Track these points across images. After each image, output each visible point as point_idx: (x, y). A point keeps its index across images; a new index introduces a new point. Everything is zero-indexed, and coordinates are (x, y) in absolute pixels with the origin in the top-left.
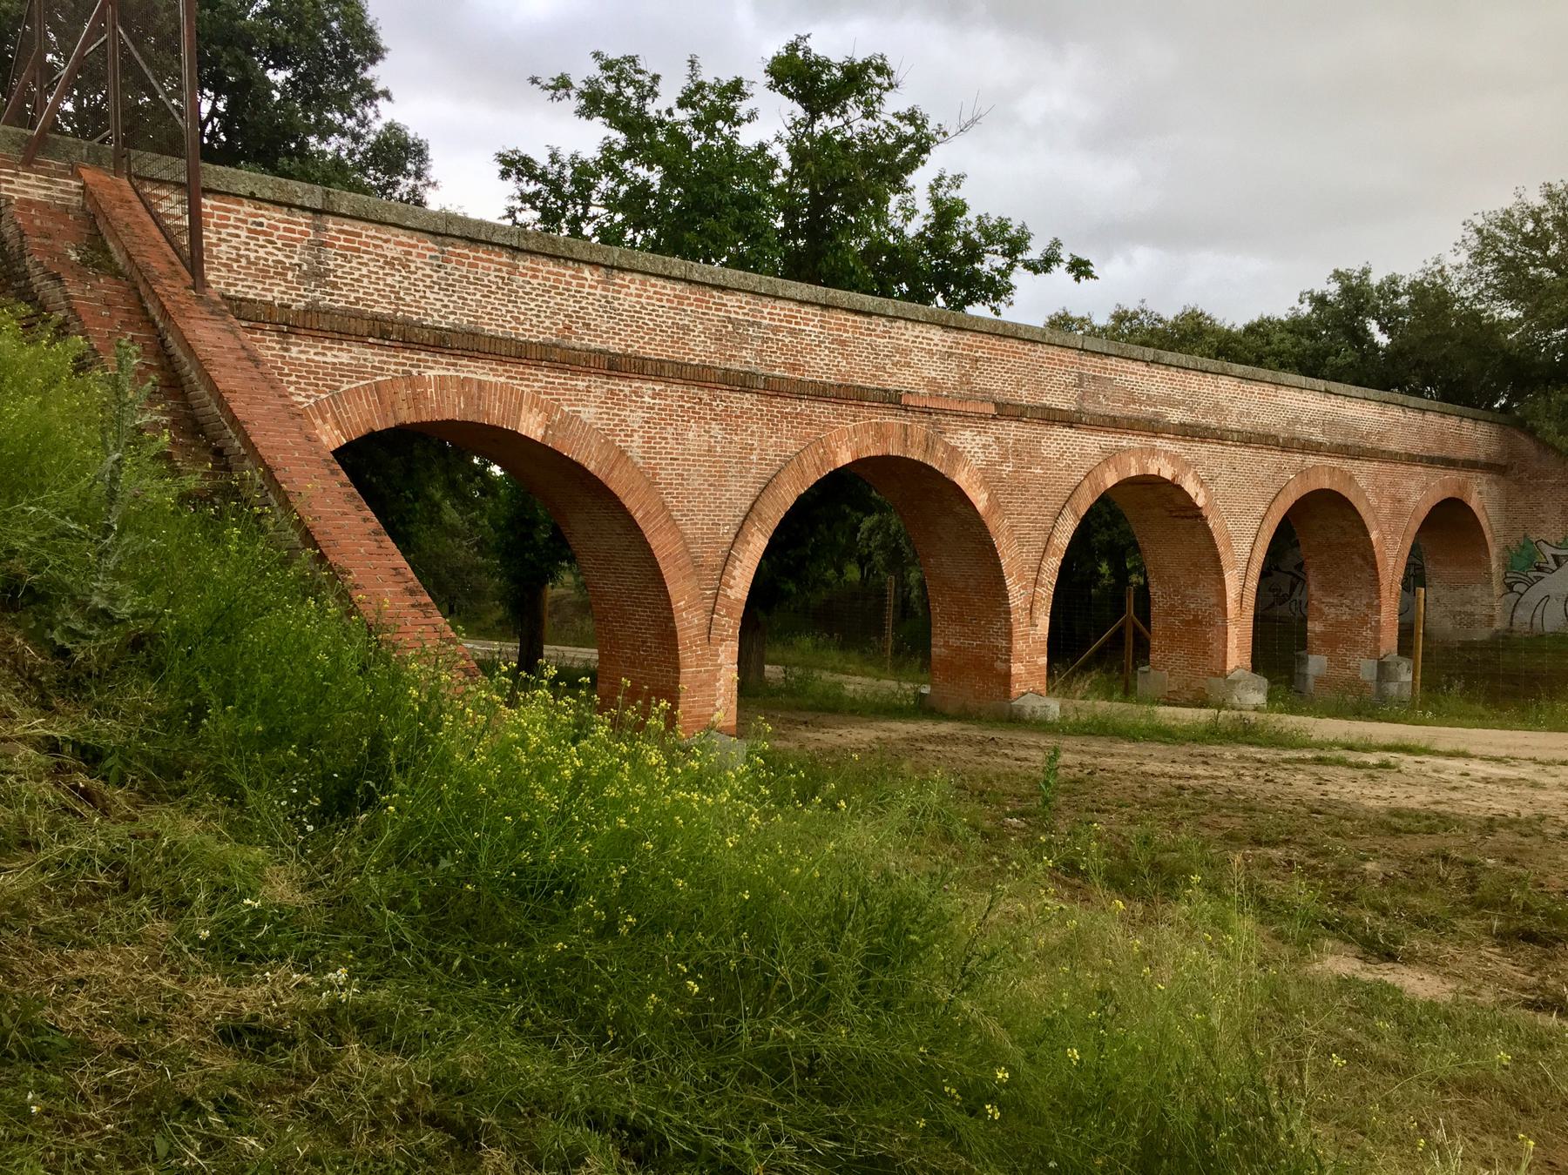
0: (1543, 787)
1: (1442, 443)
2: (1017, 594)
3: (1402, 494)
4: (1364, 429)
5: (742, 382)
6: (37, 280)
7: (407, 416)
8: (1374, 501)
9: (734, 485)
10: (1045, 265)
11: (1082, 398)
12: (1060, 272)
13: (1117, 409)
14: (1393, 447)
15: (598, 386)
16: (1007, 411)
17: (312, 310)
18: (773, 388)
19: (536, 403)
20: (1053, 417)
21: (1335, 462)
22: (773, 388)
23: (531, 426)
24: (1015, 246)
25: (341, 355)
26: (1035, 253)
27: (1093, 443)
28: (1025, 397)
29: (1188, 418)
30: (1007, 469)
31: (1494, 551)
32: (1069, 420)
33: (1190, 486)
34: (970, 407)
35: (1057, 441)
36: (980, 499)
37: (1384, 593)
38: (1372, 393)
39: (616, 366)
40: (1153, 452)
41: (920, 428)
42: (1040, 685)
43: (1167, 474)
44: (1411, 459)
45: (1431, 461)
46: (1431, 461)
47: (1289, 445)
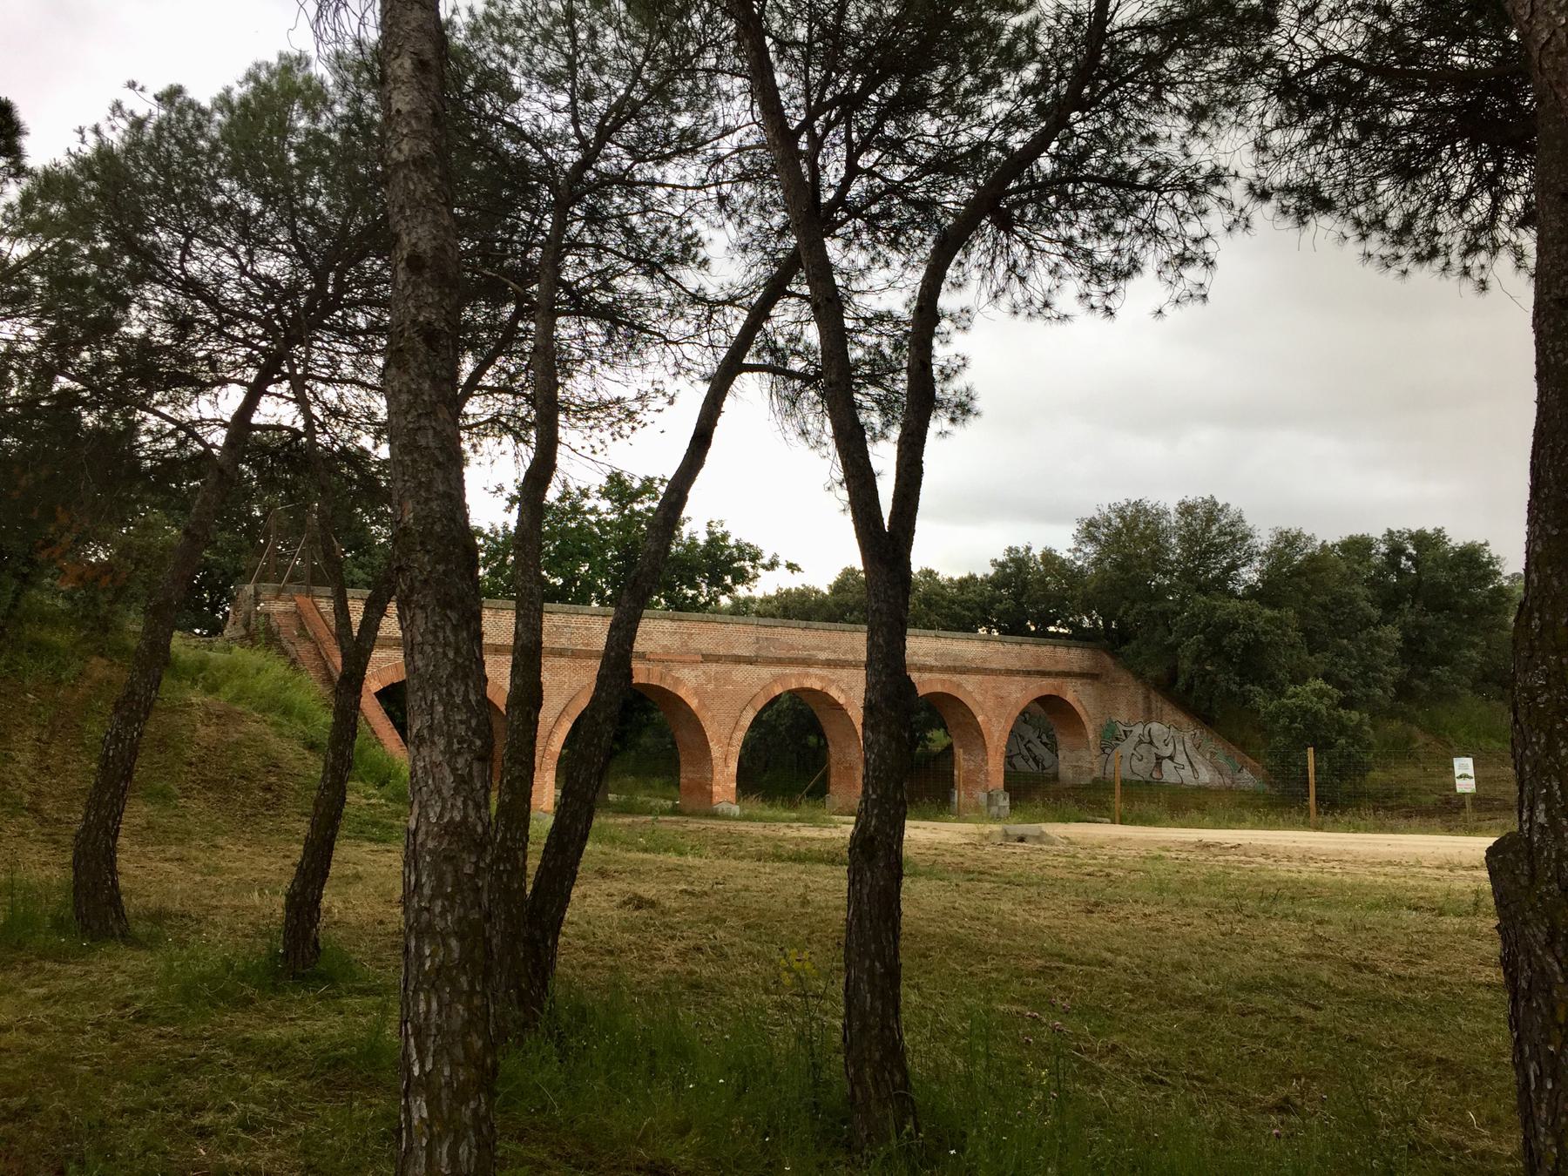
0: (1329, 922)
1: (1039, 662)
2: (716, 751)
3: (1003, 693)
4: (970, 656)
6: (285, 643)
8: (979, 698)
10: (773, 565)
11: (759, 649)
12: (781, 570)
13: (782, 654)
14: (994, 666)
16: (708, 658)
20: (738, 660)
21: (946, 677)
24: (755, 557)
26: (765, 561)
27: (766, 672)
28: (722, 651)
29: (832, 656)
30: (711, 687)
31: (1090, 728)
32: (750, 661)
33: (834, 692)
34: (686, 658)
35: (741, 673)
36: (693, 703)
37: (991, 752)
38: (958, 634)
40: (807, 675)
41: (657, 669)
42: (732, 798)
43: (817, 686)
44: (1010, 672)
45: (1028, 673)
46: (1028, 673)
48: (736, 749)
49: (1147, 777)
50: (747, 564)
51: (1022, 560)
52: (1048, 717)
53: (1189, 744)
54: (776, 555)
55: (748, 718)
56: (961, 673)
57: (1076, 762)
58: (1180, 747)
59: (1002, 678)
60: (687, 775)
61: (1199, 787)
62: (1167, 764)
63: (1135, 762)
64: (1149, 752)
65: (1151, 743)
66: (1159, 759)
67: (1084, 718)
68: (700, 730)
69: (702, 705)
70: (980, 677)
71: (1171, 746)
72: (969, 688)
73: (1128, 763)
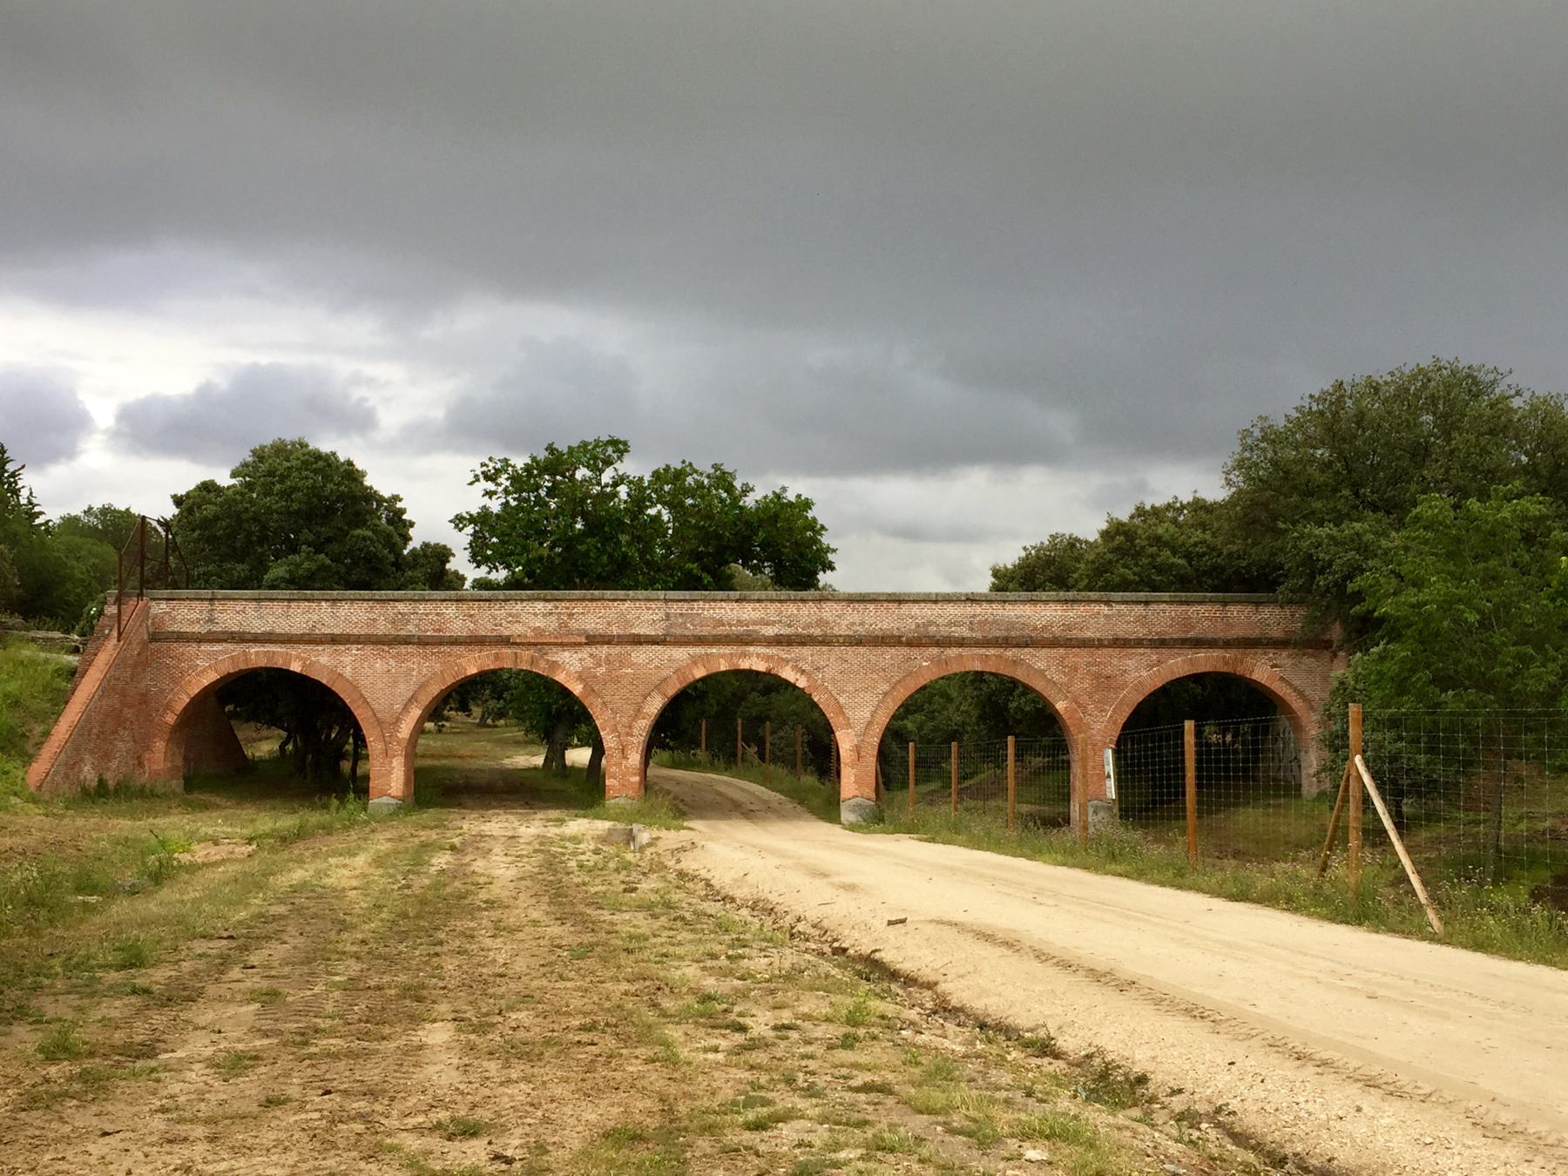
5: (406, 641)
7: (243, 667)
9: (402, 686)
15: (329, 649)
16: (593, 640)
17: (209, 632)
18: (423, 642)
19: (298, 657)
20: (638, 641)
21: (983, 651)
22: (423, 642)
23: (296, 667)
25: (218, 647)
27: (681, 654)
39: (334, 640)
47: (916, 642)
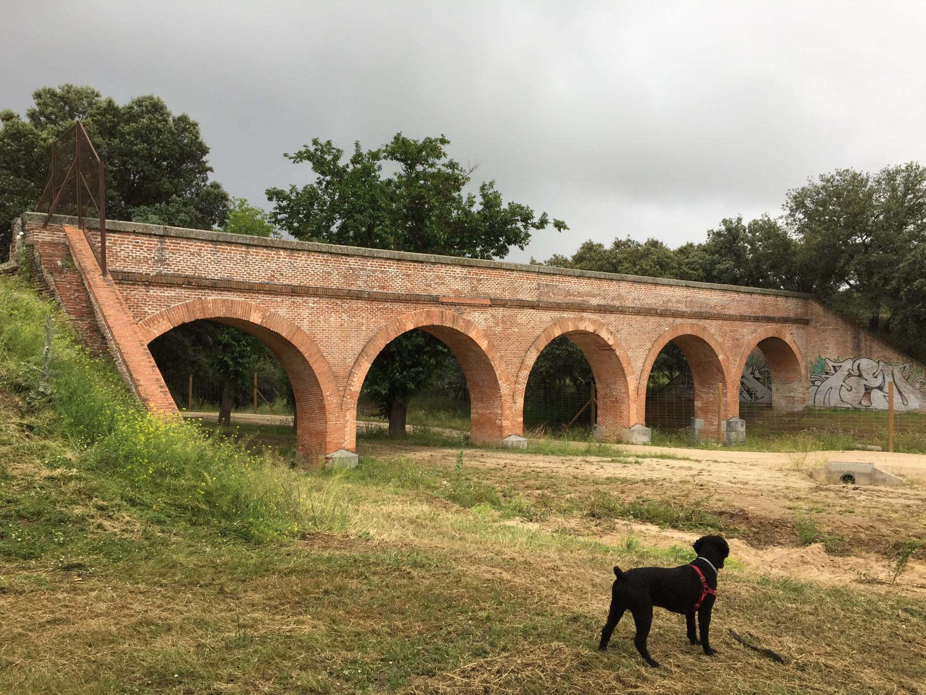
2: (504, 388)
4: (713, 304)
8: (720, 340)
10: (542, 224)
13: (560, 299)
14: (731, 312)
16: (496, 303)
20: (522, 305)
21: (694, 321)
26: (536, 220)
28: (507, 296)
30: (498, 329)
32: (533, 306)
33: (604, 335)
35: (524, 316)
36: (484, 344)
37: (729, 386)
40: (582, 319)
41: (450, 312)
43: (590, 329)
44: (743, 318)
45: (757, 319)
46: (757, 319)
48: (522, 387)
49: (856, 405)
50: (520, 225)
51: (736, 228)
52: (773, 355)
53: (898, 375)
54: (545, 214)
55: (532, 359)
56: (705, 318)
57: (790, 394)
58: (889, 379)
59: (737, 323)
60: (476, 411)
61: (909, 413)
62: (876, 394)
63: (844, 393)
64: (858, 383)
65: (860, 376)
66: (868, 390)
67: (798, 356)
68: (490, 369)
69: (492, 346)
70: (720, 322)
71: (880, 379)
72: (713, 331)
73: (837, 391)
